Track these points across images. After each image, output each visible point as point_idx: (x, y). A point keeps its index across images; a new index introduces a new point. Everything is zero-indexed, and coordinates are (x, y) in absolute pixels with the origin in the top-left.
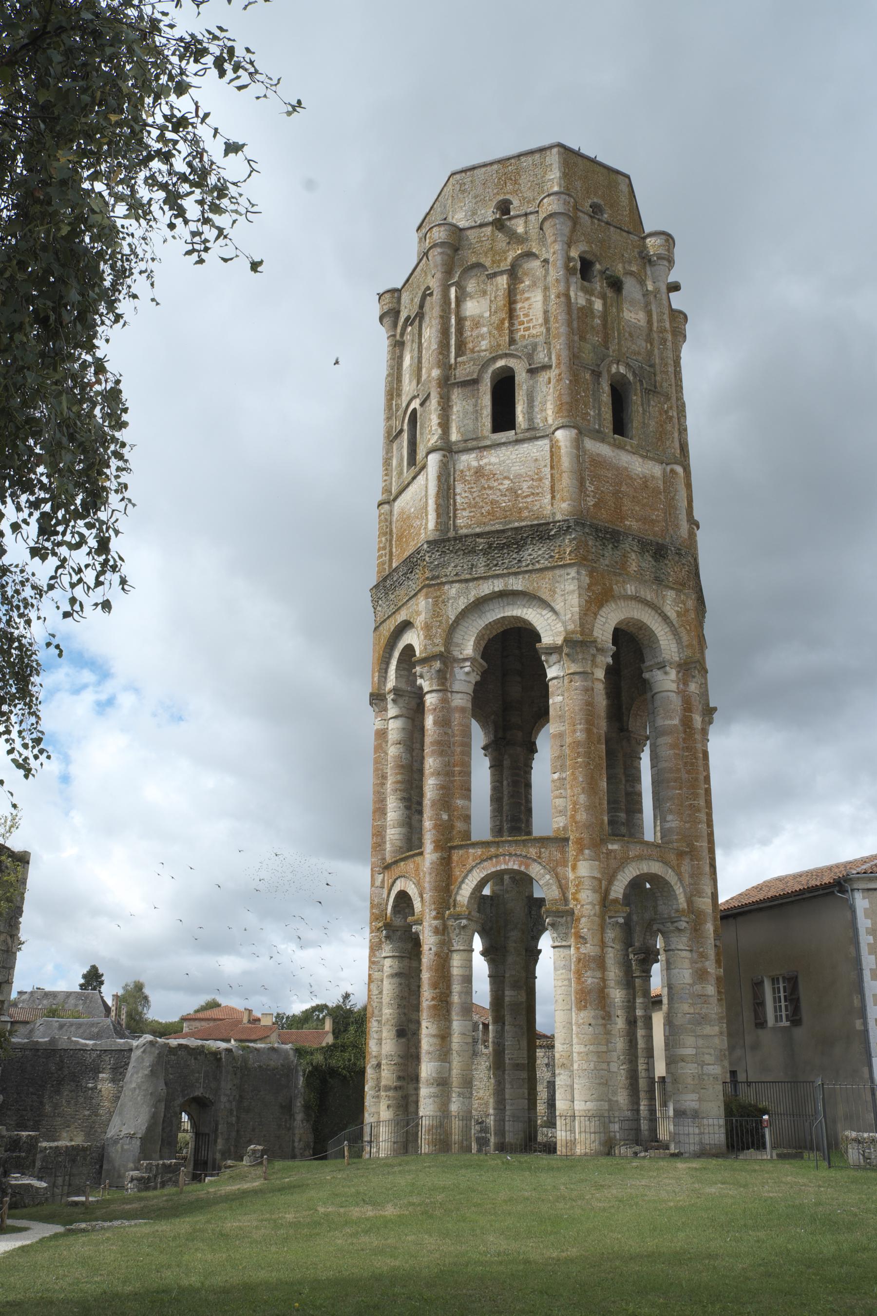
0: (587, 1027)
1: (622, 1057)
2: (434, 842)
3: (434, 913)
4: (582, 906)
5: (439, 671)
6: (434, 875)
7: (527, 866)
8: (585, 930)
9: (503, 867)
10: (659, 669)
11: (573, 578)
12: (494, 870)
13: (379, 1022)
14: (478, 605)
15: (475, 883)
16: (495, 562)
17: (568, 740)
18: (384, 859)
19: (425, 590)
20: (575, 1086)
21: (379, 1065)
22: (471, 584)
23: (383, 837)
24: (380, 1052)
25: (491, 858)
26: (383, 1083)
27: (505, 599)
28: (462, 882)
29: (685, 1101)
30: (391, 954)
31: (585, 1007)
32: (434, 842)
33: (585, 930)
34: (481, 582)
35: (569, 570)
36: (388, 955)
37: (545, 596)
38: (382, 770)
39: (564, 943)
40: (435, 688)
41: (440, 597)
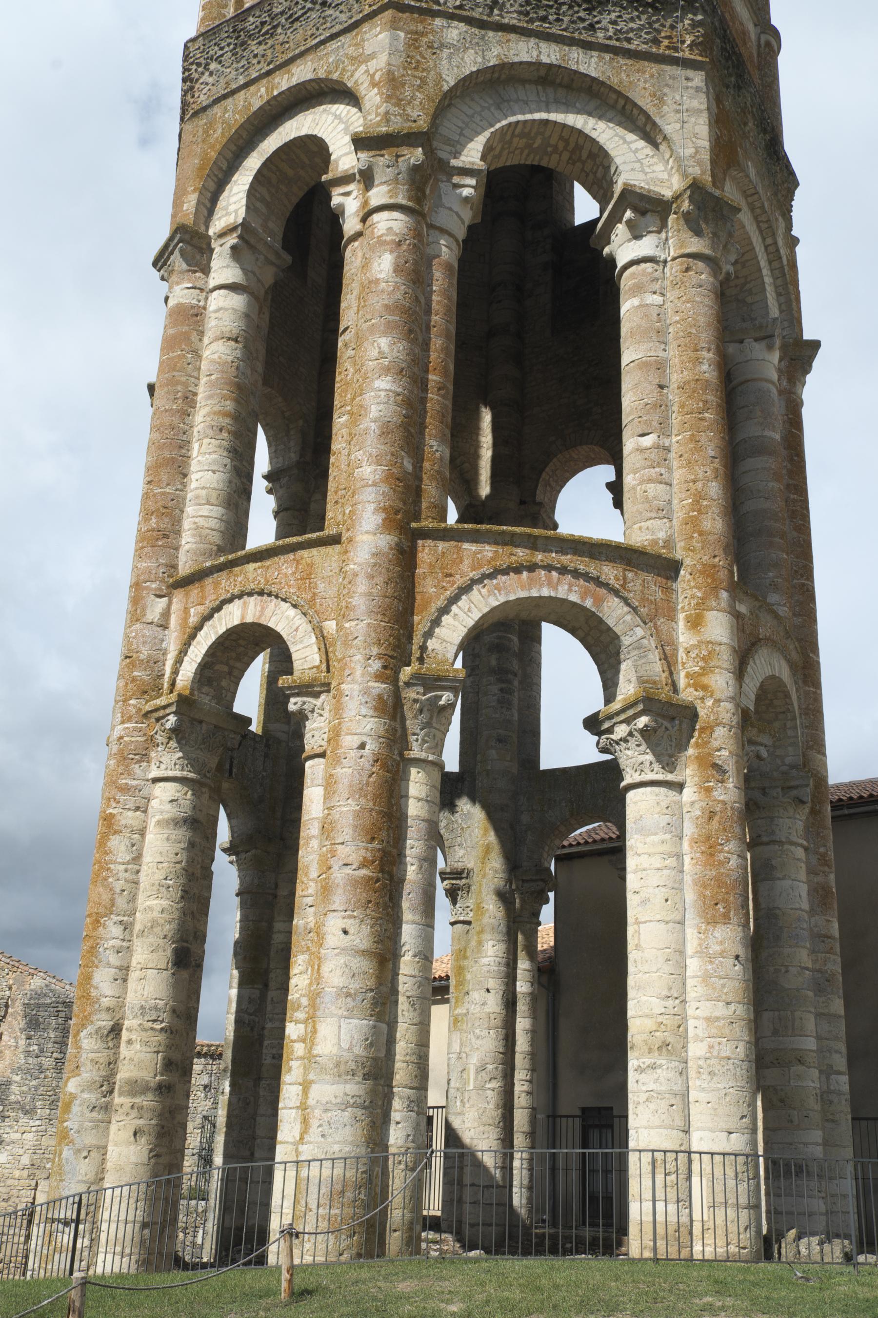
0: (732, 961)
1: (490, 1067)
2: (384, 509)
3: (376, 665)
4: (718, 701)
5: (415, 170)
6: (380, 580)
7: (599, 601)
8: (725, 753)
9: (546, 592)
10: (756, 340)
11: (698, 89)
13: (127, 927)
14: (495, 84)
15: (476, 615)
16: (542, 13)
17: (675, 378)
18: (174, 567)
19: (389, 13)
20: (693, 1095)
21: (116, 1030)
22: (491, 34)
23: (177, 522)
24: (120, 998)
25: (518, 570)
26: (124, 1073)
27: (550, 91)
28: (445, 610)
29: (806, 1144)
30: (178, 774)
31: (726, 917)
32: (384, 509)
33: (725, 753)
34: (513, 36)
35: (690, 73)
36: (170, 774)
37: (644, 102)
38: (186, 385)
39: (670, 777)
40: (401, 200)
41: (422, 34)
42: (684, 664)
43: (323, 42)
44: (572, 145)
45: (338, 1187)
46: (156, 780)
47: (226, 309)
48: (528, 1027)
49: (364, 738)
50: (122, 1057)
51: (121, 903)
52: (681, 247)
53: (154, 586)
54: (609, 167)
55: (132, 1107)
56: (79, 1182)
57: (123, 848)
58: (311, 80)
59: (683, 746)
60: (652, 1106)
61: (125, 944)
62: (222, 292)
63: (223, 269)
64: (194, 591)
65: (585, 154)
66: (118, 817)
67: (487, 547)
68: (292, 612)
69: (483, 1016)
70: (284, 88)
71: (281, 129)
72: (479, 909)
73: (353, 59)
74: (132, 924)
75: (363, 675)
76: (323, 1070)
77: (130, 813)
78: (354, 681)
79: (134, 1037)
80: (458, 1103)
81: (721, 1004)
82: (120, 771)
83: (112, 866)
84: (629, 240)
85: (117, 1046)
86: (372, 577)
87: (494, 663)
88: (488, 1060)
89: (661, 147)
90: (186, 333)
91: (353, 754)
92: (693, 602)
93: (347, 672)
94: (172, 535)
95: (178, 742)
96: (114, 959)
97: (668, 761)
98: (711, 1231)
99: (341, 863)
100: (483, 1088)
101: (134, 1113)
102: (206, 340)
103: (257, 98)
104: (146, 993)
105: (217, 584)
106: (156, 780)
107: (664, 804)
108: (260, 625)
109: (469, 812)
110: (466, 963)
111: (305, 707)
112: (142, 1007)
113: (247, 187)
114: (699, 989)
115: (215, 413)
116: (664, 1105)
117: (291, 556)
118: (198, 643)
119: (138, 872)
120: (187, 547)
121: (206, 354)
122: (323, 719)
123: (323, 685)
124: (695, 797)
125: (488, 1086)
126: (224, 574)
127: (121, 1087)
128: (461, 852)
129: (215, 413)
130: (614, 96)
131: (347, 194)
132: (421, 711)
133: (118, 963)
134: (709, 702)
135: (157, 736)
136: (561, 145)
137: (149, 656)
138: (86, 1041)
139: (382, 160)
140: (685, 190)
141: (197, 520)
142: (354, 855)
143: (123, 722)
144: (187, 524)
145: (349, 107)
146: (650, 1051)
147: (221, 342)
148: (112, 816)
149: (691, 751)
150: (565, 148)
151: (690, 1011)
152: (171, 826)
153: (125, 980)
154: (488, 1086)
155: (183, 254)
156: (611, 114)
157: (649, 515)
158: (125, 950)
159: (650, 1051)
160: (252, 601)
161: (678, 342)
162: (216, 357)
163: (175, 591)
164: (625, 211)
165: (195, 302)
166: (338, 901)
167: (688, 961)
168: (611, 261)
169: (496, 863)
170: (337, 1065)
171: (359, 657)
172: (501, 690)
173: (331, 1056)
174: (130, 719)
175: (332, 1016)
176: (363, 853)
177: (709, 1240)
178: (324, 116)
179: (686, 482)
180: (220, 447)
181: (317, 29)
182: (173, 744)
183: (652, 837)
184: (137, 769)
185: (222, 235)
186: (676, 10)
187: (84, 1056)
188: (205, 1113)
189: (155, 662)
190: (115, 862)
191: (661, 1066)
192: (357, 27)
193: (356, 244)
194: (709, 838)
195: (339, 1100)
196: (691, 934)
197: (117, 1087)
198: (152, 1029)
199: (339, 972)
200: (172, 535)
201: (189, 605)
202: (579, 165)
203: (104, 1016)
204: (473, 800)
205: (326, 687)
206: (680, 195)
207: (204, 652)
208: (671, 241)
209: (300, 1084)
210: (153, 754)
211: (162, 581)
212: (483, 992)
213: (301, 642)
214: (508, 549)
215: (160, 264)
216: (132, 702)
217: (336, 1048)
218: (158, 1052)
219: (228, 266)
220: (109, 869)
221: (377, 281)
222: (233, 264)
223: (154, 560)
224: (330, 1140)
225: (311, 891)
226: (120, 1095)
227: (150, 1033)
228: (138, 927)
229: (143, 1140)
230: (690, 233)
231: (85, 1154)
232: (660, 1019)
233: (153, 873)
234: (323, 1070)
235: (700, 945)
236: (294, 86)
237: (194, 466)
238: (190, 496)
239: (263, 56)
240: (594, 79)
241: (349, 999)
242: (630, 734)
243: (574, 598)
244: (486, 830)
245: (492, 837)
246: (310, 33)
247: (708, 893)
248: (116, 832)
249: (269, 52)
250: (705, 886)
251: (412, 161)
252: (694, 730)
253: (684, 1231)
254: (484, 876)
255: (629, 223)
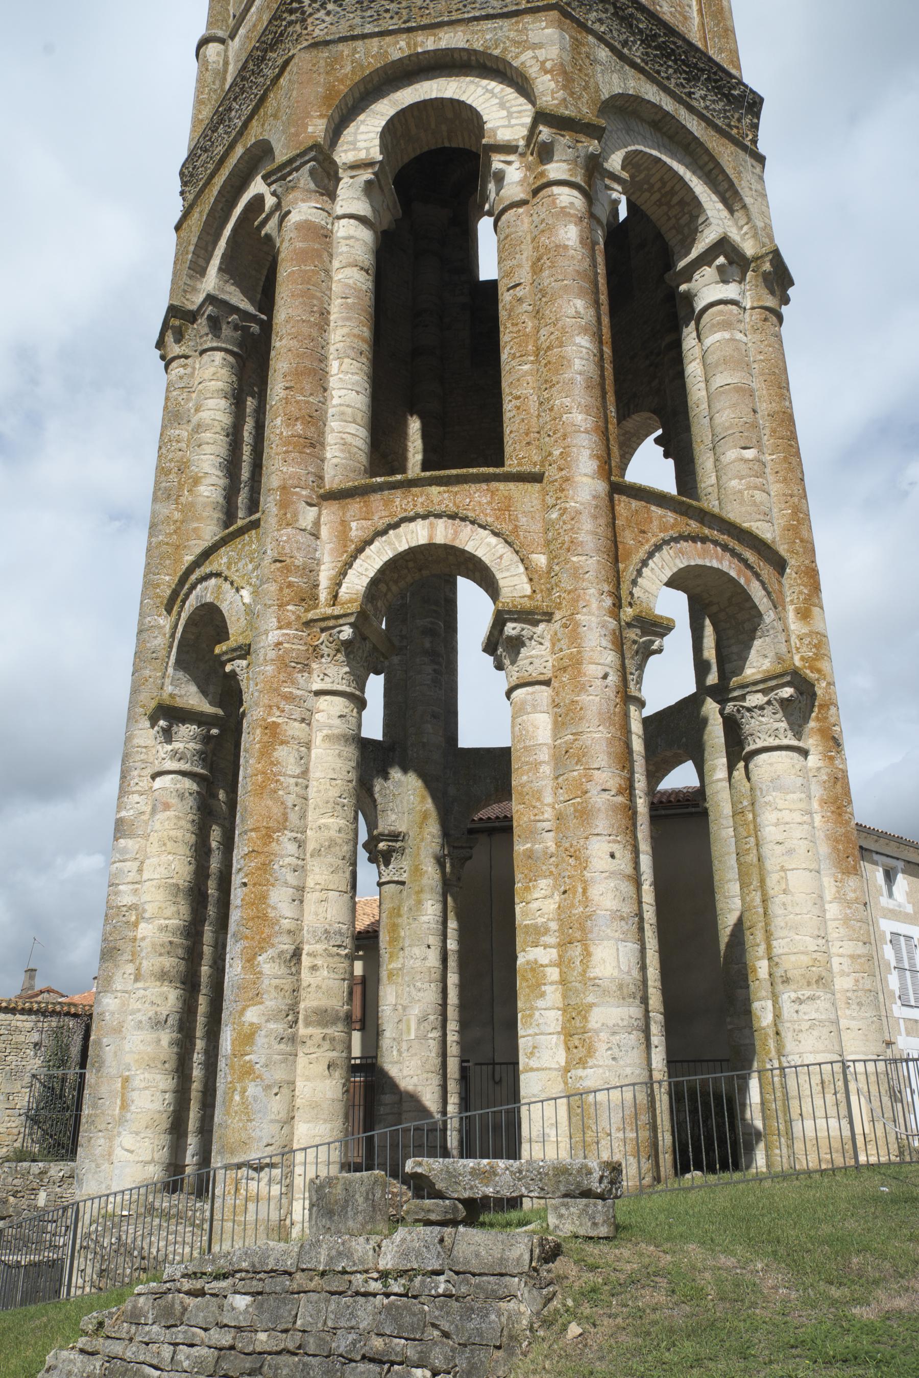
1: (432, 1018)
9: (715, 564)
12: (700, 562)
20: (843, 1023)
21: (297, 954)
36: (336, 687)
38: (322, 303)
40: (579, 179)
42: (797, 649)
43: (476, 19)
44: (667, 188)
45: (629, 1111)
46: (319, 693)
47: (358, 240)
48: (457, 982)
49: (608, 669)
50: (304, 984)
51: (293, 817)
52: (759, 300)
53: (304, 493)
54: (698, 217)
55: (324, 1038)
56: (272, 1121)
57: (292, 760)
58: (463, 49)
59: (806, 719)
60: (815, 1033)
61: (300, 862)
62: (352, 221)
63: (351, 197)
64: (355, 506)
65: (675, 200)
66: (284, 727)
67: (669, 514)
68: (493, 540)
69: (424, 970)
70: (430, 48)
71: (417, 86)
72: (417, 871)
73: (517, 43)
74: (304, 842)
75: (599, 608)
76: (605, 992)
77: (296, 724)
78: (590, 613)
79: (319, 962)
80: (395, 1053)
81: (861, 944)
82: (282, 678)
83: (282, 778)
84: (717, 283)
85: (299, 972)
86: (595, 517)
87: (427, 645)
88: (430, 1011)
89: (736, 214)
90: (317, 250)
91: (599, 682)
92: (802, 597)
93: (581, 603)
94: (318, 446)
95: (347, 656)
96: (291, 878)
97: (797, 729)
98: (873, 1143)
99: (599, 788)
100: (425, 1038)
101: (326, 1045)
102: (336, 264)
103: (398, 49)
104: (329, 916)
105: (387, 503)
106: (319, 693)
107: (798, 767)
108: (453, 548)
109: (400, 780)
110: (400, 920)
111: (524, 633)
112: (326, 932)
113: (380, 129)
114: (841, 930)
115: (354, 336)
116: (825, 1031)
117: (484, 486)
118: (368, 557)
119: (307, 787)
120: (335, 461)
121: (337, 276)
122: (543, 647)
123: (545, 614)
124: (820, 764)
125: (430, 1035)
126: (398, 493)
127: (306, 1017)
128: (393, 817)
129: (354, 336)
130: (706, 158)
131: (509, 163)
132: (637, 652)
133: (295, 883)
134: (824, 684)
135: (323, 647)
136: (659, 185)
137: (304, 563)
138: (267, 966)
139: (565, 140)
140: (767, 254)
141: (344, 436)
142: (612, 782)
143: (280, 628)
144: (330, 438)
145: (501, 86)
146: (809, 984)
147: (355, 269)
148: (276, 725)
149: (812, 724)
150: (659, 190)
151: (834, 950)
152: (342, 742)
153: (302, 902)
154: (430, 1035)
155: (312, 173)
156: (699, 172)
157: (758, 517)
158: (300, 869)
159: (809, 984)
160: (441, 523)
161: (765, 377)
162: (351, 281)
163: (325, 503)
164: (717, 257)
165: (323, 223)
166: (601, 826)
167: (827, 906)
168: (689, 298)
169: (433, 828)
170: (620, 987)
171: (592, 591)
172: (435, 670)
173: (613, 979)
174: (289, 625)
175: (609, 938)
176: (618, 780)
177: (872, 1150)
178: (472, 87)
179: (784, 495)
180: (361, 370)
181: (465, 6)
182: (341, 657)
183: (791, 795)
184: (300, 678)
185: (355, 166)
186: (742, 108)
187: (266, 982)
188: (33, 1071)
189: (310, 571)
190: (285, 775)
191: (819, 998)
192: (517, 16)
193: (521, 210)
194: (837, 798)
195: (625, 1023)
196: (828, 883)
197: (301, 1017)
198: (338, 954)
199: (610, 895)
200: (318, 446)
201: (348, 518)
202: (665, 208)
203: (285, 938)
204: (405, 771)
205: (548, 617)
206: (762, 257)
207: (378, 567)
208: (748, 293)
209: (559, 1009)
210: (314, 666)
211: (312, 490)
212: (424, 948)
213: (508, 570)
214: (685, 519)
215: (274, 178)
216: (290, 607)
217: (616, 970)
218: (344, 980)
219: (358, 199)
220: (277, 781)
221: (566, 247)
222: (363, 198)
223: (303, 466)
224: (621, 1063)
225: (546, 816)
226: (307, 1024)
227: (337, 959)
228: (311, 846)
229: (337, 1074)
230: (767, 291)
231: (276, 1090)
232: (815, 955)
233: (326, 790)
234: (605, 992)
235: (838, 892)
236: (442, 50)
237: (333, 382)
238: (331, 411)
239: (397, 13)
240: (696, 138)
241: (623, 923)
242: (769, 703)
243: (733, 574)
244: (423, 797)
245: (429, 804)
246: (455, 7)
247: (840, 847)
248: (282, 743)
249: (404, 12)
250: (837, 841)
251: (591, 149)
252: (813, 706)
253: (849, 1146)
254: (422, 840)
255: (720, 269)
